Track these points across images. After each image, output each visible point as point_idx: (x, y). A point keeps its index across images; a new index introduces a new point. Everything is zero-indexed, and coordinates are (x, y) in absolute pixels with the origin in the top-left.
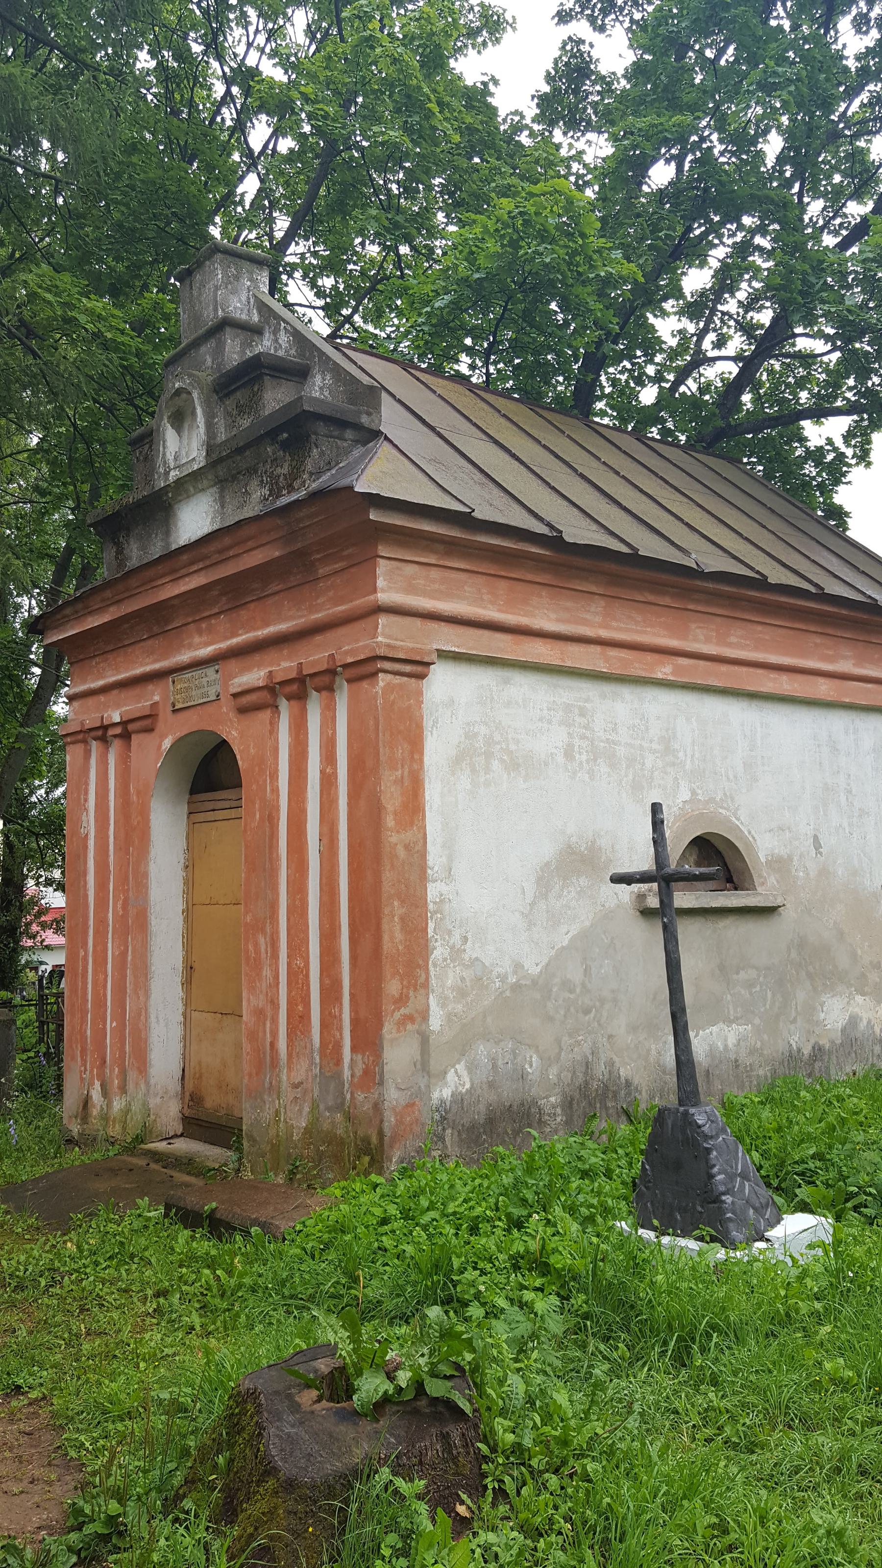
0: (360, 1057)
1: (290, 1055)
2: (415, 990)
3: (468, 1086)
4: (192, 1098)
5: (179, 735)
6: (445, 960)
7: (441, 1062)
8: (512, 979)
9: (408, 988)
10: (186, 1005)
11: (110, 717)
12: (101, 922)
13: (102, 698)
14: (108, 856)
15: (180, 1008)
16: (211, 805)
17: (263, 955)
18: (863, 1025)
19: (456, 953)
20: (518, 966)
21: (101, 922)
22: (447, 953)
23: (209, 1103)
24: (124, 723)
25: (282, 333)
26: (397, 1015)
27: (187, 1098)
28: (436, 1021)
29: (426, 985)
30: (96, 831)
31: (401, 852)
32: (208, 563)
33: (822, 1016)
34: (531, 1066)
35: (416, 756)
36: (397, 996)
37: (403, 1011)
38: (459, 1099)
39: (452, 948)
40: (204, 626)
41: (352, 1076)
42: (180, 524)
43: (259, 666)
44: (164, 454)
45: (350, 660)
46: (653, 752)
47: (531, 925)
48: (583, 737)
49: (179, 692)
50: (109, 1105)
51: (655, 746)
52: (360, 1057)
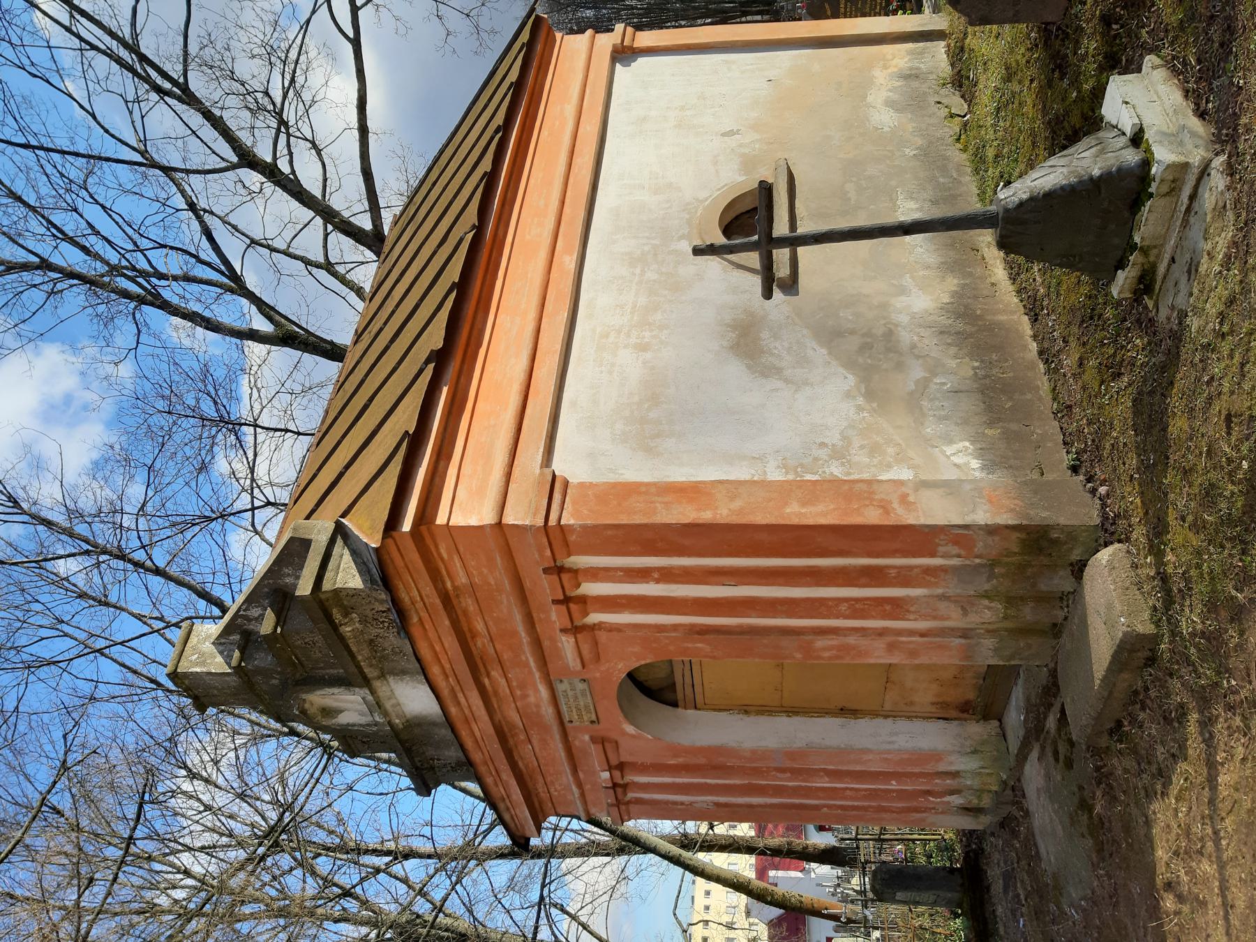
0: (941, 549)
1: (935, 618)
2: (873, 493)
3: (967, 444)
4: (966, 710)
5: (621, 718)
6: (843, 464)
7: (944, 471)
8: (861, 401)
9: (872, 500)
10: (877, 716)
11: (605, 781)
12: (796, 792)
13: (587, 787)
14: (735, 785)
15: (880, 720)
16: (689, 690)
17: (835, 642)
18: (895, 97)
19: (838, 454)
20: (848, 395)
21: (796, 792)
22: (835, 463)
23: (971, 695)
24: (610, 769)
25: (249, 613)
26: (900, 510)
27: (965, 715)
28: (905, 474)
29: (869, 482)
30: (711, 794)
31: (737, 504)
32: (457, 688)
33: (886, 129)
34: (944, 384)
35: (643, 489)
36: (881, 511)
37: (895, 505)
38: (981, 453)
39: (831, 457)
40: (519, 693)
41: (959, 556)
42: (424, 713)
43: (553, 640)
44: (361, 725)
45: (548, 553)
46: (643, 272)
47: (806, 383)
48: (628, 336)
49: (580, 716)
50: (970, 788)
51: (638, 271)
52: (941, 549)
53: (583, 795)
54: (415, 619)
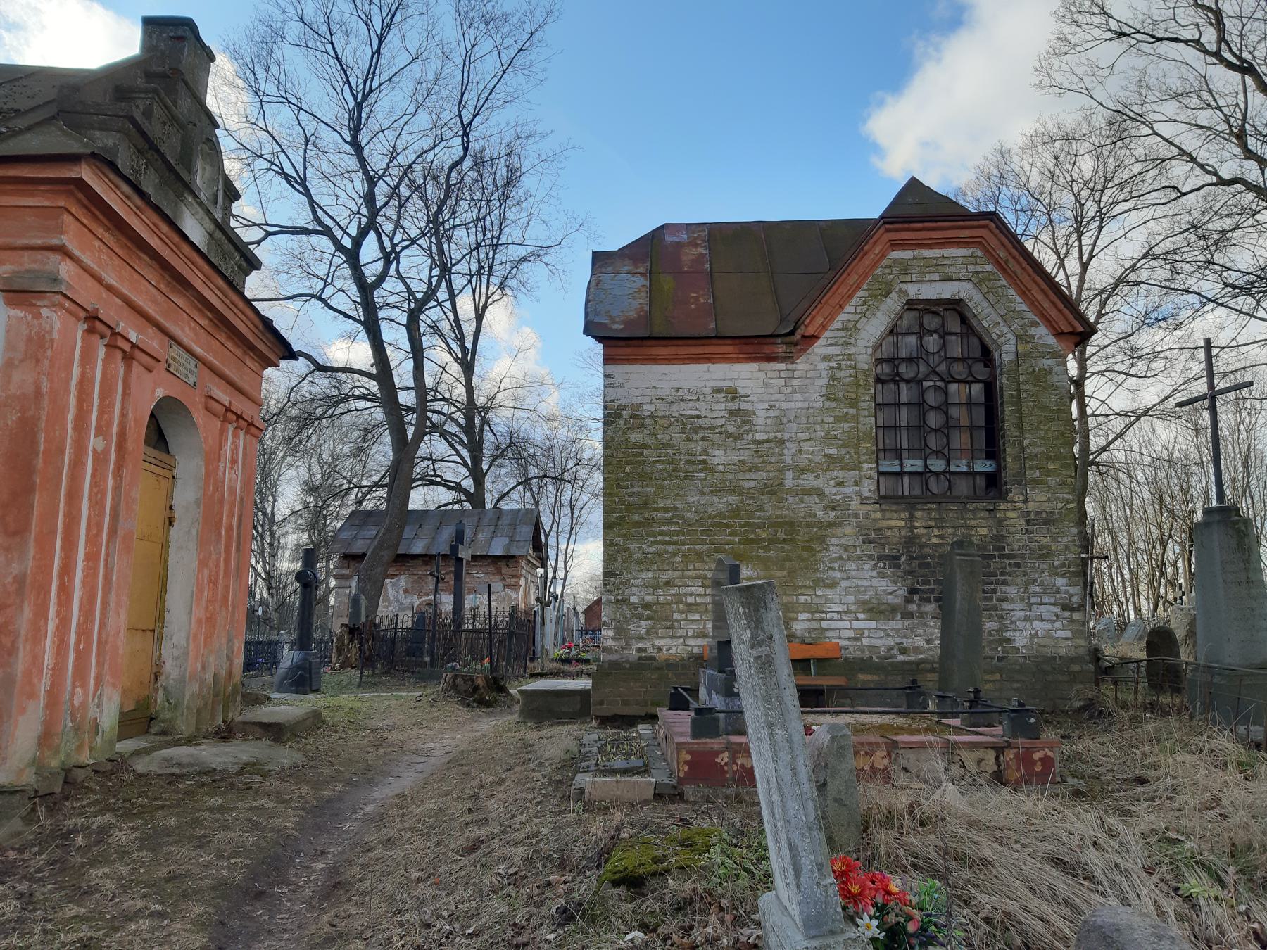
53: (99, 280)
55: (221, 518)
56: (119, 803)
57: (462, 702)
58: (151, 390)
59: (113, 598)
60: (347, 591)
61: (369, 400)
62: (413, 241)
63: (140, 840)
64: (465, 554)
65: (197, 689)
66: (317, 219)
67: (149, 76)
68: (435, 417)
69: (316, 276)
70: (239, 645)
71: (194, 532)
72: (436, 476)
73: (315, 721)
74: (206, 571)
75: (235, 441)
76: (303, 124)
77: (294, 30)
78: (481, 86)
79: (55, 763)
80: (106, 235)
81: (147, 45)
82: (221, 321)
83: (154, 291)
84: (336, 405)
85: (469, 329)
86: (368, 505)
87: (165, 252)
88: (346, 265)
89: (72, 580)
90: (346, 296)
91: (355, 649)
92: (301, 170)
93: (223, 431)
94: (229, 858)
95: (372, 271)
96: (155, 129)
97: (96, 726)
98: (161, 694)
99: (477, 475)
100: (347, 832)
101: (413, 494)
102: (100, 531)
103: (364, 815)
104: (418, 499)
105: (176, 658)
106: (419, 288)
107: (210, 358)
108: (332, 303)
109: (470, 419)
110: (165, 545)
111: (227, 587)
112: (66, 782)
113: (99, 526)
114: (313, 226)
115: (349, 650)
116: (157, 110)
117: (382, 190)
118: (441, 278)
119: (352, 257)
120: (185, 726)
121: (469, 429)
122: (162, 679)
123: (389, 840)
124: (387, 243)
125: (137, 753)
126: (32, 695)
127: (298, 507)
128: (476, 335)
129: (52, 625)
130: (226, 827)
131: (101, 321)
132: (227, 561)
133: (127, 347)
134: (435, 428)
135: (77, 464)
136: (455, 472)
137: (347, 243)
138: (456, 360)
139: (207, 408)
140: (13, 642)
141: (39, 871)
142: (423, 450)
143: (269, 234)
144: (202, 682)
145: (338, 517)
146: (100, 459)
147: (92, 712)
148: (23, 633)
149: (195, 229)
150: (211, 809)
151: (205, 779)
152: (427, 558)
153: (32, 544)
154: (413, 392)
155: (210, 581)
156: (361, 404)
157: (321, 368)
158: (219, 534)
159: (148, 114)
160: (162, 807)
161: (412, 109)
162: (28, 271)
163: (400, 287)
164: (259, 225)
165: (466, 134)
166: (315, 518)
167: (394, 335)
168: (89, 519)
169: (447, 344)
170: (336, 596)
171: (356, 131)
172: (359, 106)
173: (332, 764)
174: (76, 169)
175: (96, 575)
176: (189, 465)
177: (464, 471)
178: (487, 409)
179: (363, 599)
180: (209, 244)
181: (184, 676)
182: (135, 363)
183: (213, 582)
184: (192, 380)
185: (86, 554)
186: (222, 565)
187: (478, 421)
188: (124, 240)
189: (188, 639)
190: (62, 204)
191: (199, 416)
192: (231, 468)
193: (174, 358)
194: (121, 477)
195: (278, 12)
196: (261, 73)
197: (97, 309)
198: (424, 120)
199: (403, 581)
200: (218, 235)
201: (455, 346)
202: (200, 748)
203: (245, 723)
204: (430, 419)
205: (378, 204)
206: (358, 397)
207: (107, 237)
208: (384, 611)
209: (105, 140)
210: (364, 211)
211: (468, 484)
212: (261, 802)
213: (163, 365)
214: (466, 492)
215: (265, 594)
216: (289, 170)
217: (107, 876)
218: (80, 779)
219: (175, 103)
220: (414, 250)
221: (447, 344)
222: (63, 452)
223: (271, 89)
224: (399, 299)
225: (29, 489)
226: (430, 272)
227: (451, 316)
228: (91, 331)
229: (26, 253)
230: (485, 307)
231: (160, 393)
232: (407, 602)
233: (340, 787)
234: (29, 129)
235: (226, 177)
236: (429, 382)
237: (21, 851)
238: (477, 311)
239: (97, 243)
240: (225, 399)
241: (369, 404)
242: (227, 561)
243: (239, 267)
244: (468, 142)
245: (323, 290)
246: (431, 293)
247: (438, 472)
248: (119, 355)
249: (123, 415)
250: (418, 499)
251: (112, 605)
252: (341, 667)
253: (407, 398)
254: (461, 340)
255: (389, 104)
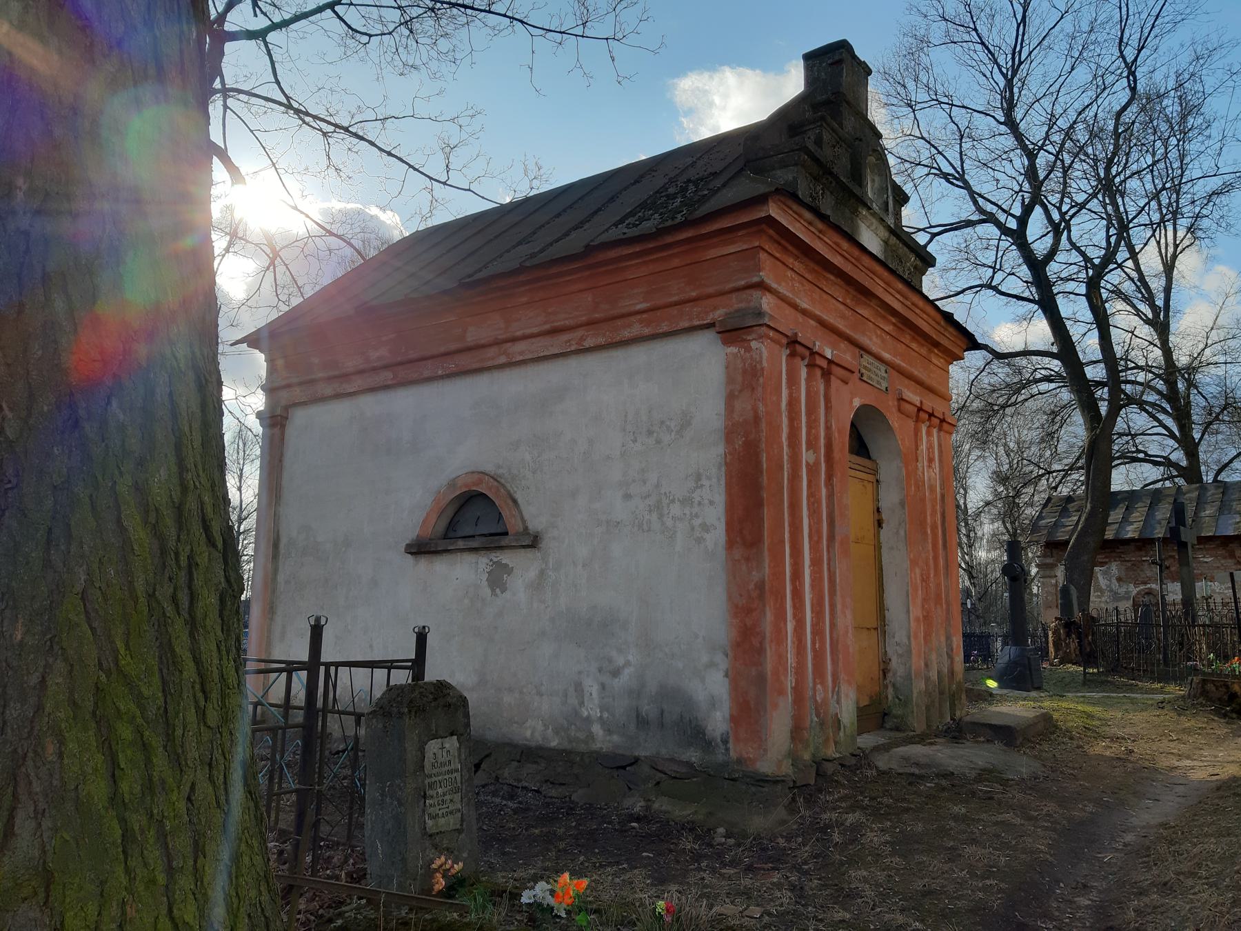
53: (795, 306)
54: (942, 323)
55: (925, 517)
56: (866, 801)
57: (1217, 712)
58: (849, 401)
59: (838, 599)
60: (1053, 581)
61: (1052, 381)
62: (1082, 206)
63: (892, 844)
64: (1187, 535)
65: (923, 686)
66: (980, 210)
67: (815, 107)
68: (1128, 388)
69: (984, 265)
70: (958, 642)
71: (902, 533)
72: (1139, 451)
73: (1046, 727)
74: (918, 571)
75: (929, 439)
76: (956, 120)
77: (938, 31)
78: (1144, 16)
79: (807, 756)
80: (796, 263)
81: (810, 80)
82: (906, 324)
83: (842, 307)
84: (1018, 391)
85: (1157, 285)
86: (1064, 491)
87: (848, 269)
88: (1014, 247)
89: (802, 584)
90: (1018, 280)
91: (1074, 644)
92: (957, 164)
93: (917, 432)
94: (983, 878)
95: (1041, 248)
96: (827, 153)
97: (838, 722)
98: (890, 690)
99: (1191, 448)
100: (1109, 864)
101: (1115, 473)
102: (820, 537)
103: (1125, 845)
104: (1122, 479)
105: (900, 656)
106: (1096, 254)
107: (898, 361)
108: (1003, 288)
109: (1172, 385)
110: (878, 547)
111: (938, 585)
112: (817, 774)
113: (819, 532)
114: (975, 217)
115: (1068, 645)
116: (826, 136)
117: (1042, 160)
118: (1120, 237)
119: (1019, 237)
120: (919, 725)
121: (1172, 395)
122: (890, 675)
123: (1165, 884)
124: (1056, 216)
125: (877, 749)
126: (781, 692)
127: (990, 498)
128: (1168, 290)
129: (790, 626)
130: (974, 841)
131: (800, 344)
132: (936, 558)
133: (824, 364)
134: (1131, 400)
135: (795, 477)
136: (1161, 445)
137: (1012, 224)
138: (1147, 322)
139: (899, 410)
140: (761, 643)
141: (805, 863)
142: (1120, 425)
143: (934, 235)
144: (927, 679)
145: (1030, 504)
146: (813, 470)
147: (833, 708)
148: (768, 635)
149: (871, 239)
150: (956, 818)
151: (944, 782)
152: (1143, 543)
153: (766, 553)
154: (1102, 365)
155: (923, 580)
156: (1044, 386)
157: (999, 356)
158: (926, 533)
159: (819, 142)
160: (907, 810)
161: (1068, 67)
162: (737, 311)
163: (1075, 257)
164: (923, 230)
165: (1132, 73)
166: (1010, 509)
167: (1075, 309)
168: (810, 530)
169: (1134, 306)
170: (1042, 587)
171: (1009, 105)
172: (1009, 84)
173: (1075, 777)
174: (765, 208)
175: (821, 579)
176: (889, 469)
177: (1171, 442)
178: (1191, 369)
179: (1074, 592)
180: (885, 251)
181: (910, 674)
182: (833, 378)
183: (925, 580)
184: (884, 385)
185: (811, 560)
186: (931, 562)
187: (1181, 385)
188: (812, 265)
189: (909, 638)
190: (757, 244)
191: (894, 420)
192: (929, 466)
193: (865, 367)
194: (832, 485)
195: (920, 19)
196: (911, 85)
197: (796, 334)
198: (1083, 74)
199: (1115, 568)
200: (893, 240)
201: (1145, 309)
202: (934, 748)
203: (974, 723)
204: (1123, 392)
205: (1042, 175)
206: (1040, 380)
207: (797, 266)
208: (1099, 603)
209: (784, 176)
210: (1026, 186)
211: (1179, 456)
212: (1007, 816)
213: (857, 375)
214: (1176, 465)
215: (967, 583)
216: (947, 169)
217: (865, 880)
218: (829, 773)
219: (841, 125)
220: (1084, 216)
221: (1134, 306)
222: (782, 468)
223: (922, 96)
224: (1074, 269)
225: (759, 504)
226: (1108, 231)
227: (1134, 275)
228: (792, 355)
229: (734, 295)
230: (1175, 256)
231: (857, 403)
232: (1122, 591)
233: (1090, 808)
234: (724, 186)
235: (894, 184)
236: (1119, 351)
237: (788, 839)
238: (1165, 264)
239: (789, 273)
240: (916, 399)
241: (1053, 385)
242: (936, 558)
243: (915, 268)
244: (1135, 81)
245: (992, 278)
246: (1109, 257)
247: (1140, 447)
248: (818, 373)
249: (828, 428)
250: (1122, 479)
251: (839, 607)
252: (1061, 663)
253: (1095, 373)
254: (1150, 299)
255: (1038, 75)
